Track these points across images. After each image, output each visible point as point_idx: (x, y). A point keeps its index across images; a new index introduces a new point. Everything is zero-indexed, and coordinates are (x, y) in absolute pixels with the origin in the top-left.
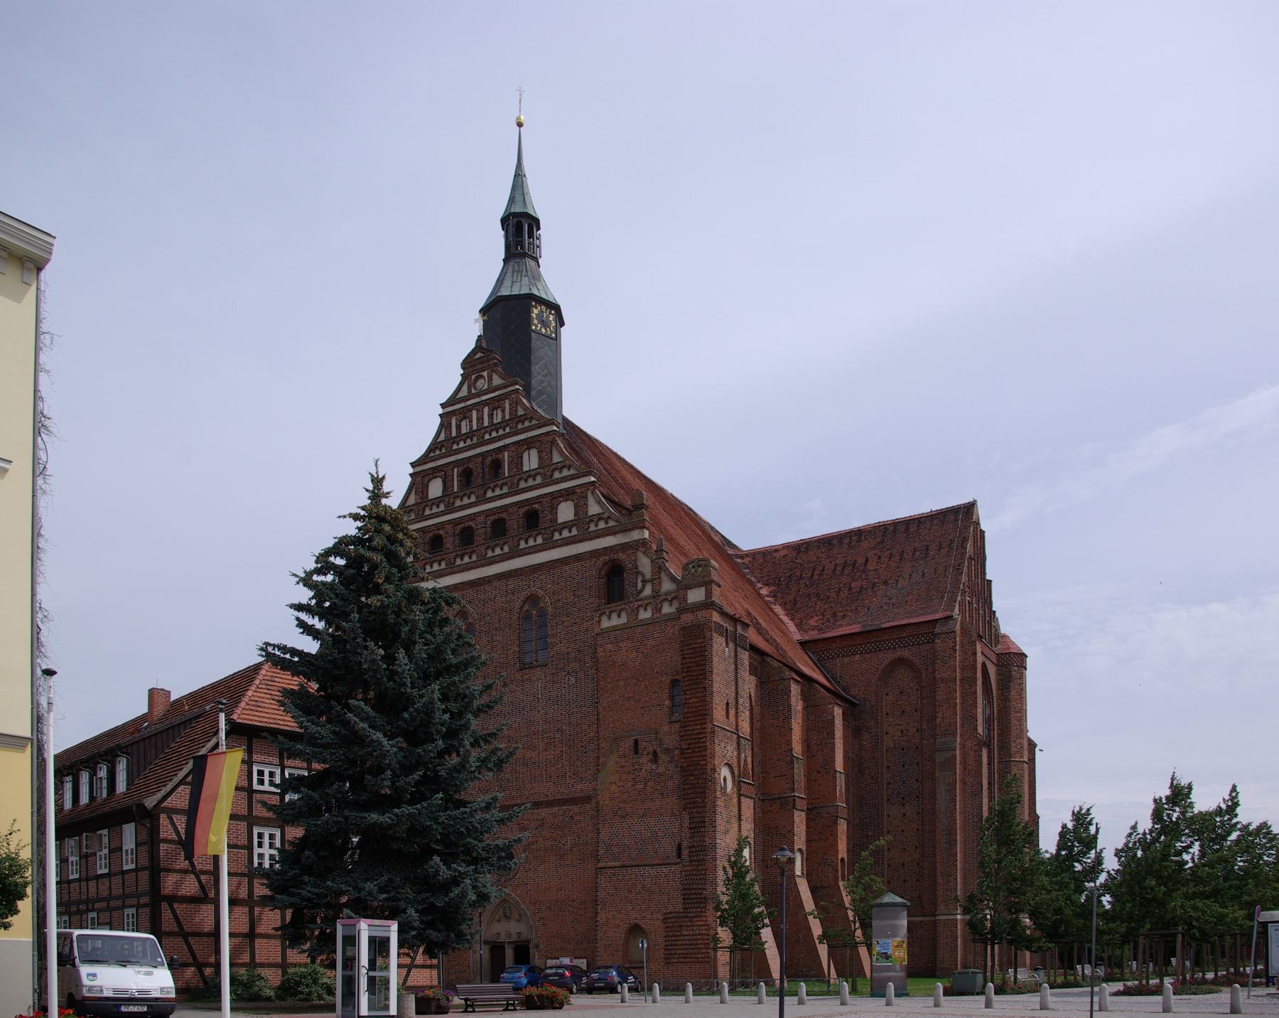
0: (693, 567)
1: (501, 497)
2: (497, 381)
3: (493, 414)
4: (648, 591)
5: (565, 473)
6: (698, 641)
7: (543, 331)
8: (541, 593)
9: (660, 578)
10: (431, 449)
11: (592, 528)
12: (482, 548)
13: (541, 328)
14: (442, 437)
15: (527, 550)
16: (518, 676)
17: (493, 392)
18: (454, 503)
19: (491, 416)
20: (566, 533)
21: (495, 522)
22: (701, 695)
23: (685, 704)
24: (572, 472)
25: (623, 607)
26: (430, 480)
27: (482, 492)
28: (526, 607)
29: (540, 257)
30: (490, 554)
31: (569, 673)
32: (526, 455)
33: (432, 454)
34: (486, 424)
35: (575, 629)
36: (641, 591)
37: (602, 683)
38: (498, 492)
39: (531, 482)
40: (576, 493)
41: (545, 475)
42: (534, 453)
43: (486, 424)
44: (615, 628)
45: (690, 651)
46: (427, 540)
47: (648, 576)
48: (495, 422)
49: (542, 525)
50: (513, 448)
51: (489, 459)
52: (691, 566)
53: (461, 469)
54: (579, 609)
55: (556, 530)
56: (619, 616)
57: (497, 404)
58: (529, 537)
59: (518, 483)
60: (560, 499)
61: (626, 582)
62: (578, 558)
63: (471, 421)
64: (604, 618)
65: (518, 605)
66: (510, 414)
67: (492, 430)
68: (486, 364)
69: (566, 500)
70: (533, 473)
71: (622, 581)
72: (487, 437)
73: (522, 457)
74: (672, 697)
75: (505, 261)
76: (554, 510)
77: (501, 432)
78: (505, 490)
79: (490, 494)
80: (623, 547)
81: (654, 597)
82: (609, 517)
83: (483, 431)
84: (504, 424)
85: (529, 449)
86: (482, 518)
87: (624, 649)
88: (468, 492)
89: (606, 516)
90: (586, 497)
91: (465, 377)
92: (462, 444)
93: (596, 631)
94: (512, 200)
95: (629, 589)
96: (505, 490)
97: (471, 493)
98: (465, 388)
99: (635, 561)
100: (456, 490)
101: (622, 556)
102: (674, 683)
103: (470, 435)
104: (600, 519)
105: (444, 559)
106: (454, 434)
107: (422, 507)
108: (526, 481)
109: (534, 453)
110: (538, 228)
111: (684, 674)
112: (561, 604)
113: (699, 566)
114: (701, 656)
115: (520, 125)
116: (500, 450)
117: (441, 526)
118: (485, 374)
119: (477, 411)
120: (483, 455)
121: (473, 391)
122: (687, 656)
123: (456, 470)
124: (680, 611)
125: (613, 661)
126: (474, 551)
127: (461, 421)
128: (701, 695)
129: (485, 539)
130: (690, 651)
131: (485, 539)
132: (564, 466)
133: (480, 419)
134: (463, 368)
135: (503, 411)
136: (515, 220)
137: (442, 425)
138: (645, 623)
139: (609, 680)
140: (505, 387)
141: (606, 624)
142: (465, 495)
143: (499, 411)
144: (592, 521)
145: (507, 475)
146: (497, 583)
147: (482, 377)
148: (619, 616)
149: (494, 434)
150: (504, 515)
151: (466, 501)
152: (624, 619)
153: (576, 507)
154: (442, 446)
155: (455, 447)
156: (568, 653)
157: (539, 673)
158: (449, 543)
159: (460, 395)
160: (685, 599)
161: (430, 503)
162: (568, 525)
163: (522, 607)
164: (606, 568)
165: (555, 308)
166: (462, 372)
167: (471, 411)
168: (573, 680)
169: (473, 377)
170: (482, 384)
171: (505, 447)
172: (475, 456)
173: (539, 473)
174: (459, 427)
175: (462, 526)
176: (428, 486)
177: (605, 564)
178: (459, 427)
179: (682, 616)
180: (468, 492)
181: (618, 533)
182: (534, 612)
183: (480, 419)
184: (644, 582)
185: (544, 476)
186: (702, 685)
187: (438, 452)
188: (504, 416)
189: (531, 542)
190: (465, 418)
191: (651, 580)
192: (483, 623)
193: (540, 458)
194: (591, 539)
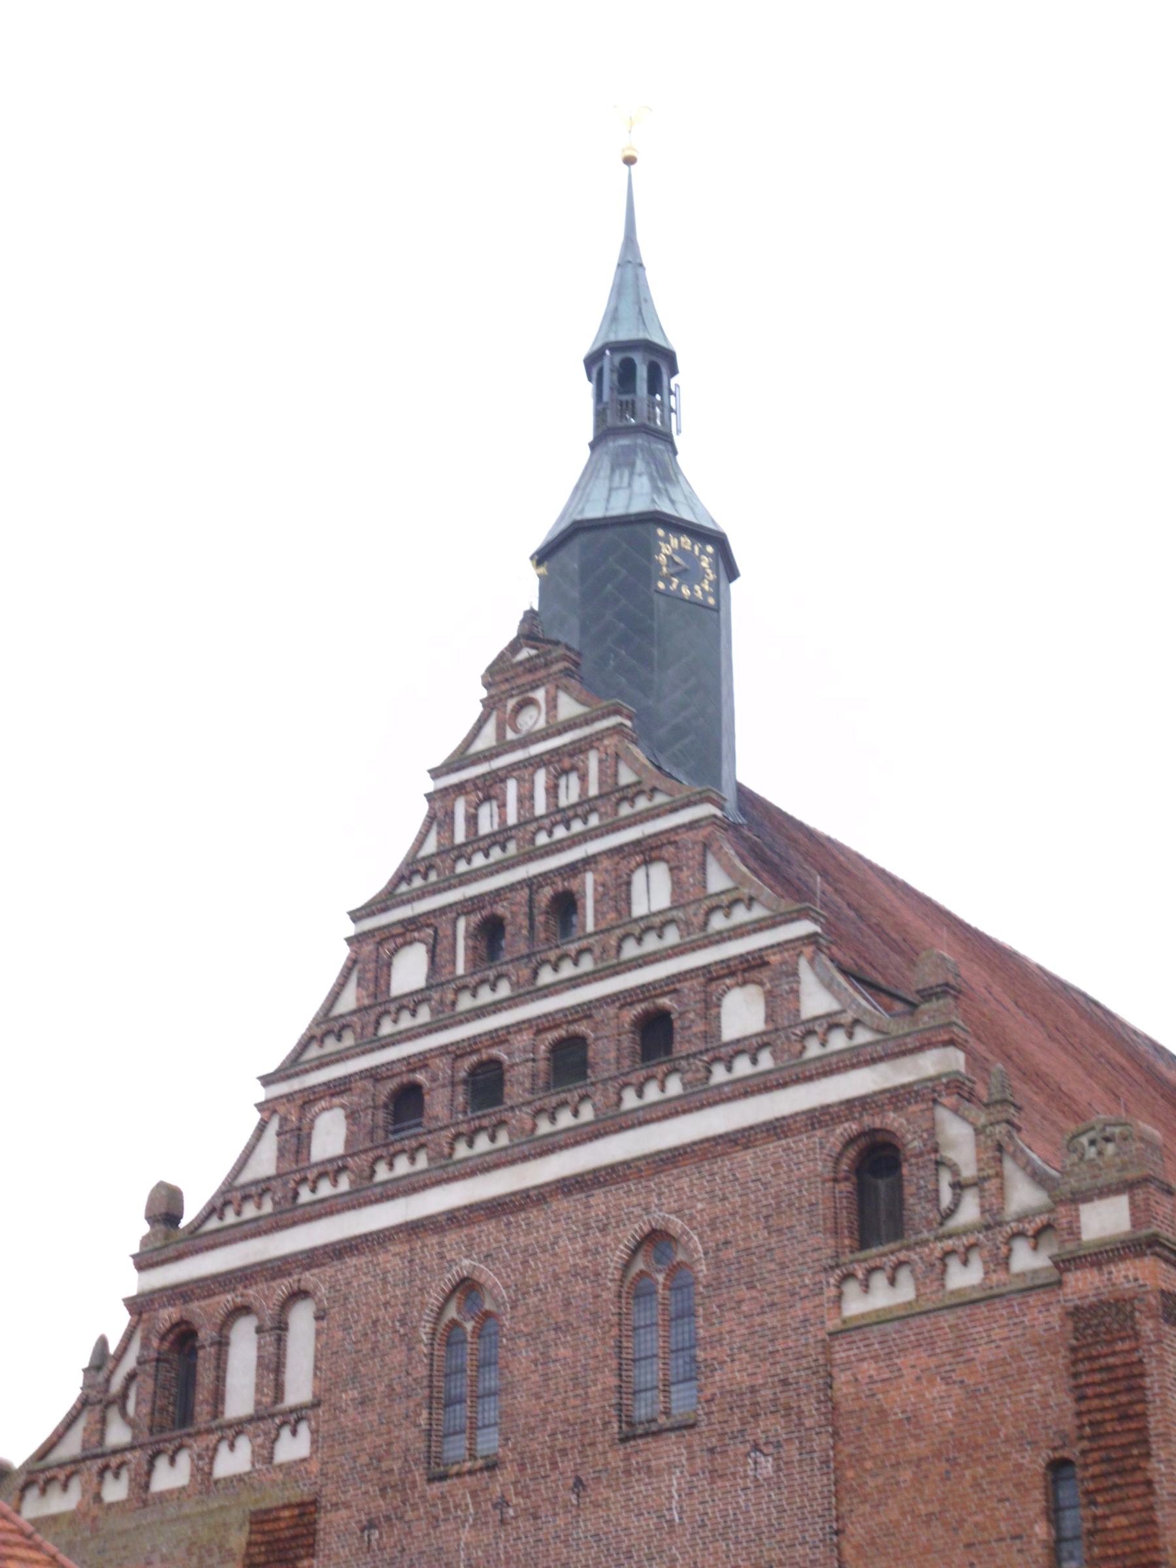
0: (1092, 1142)
1: (574, 983)
2: (568, 707)
3: (556, 787)
4: (969, 1212)
5: (741, 915)
6: (1120, 1346)
7: (686, 591)
8: (677, 1225)
9: (999, 1175)
10: (401, 877)
11: (813, 1049)
12: (525, 1114)
13: (679, 586)
14: (430, 847)
15: (641, 1113)
16: (615, 1459)
17: (559, 732)
18: (454, 1004)
19: (553, 791)
20: (743, 1067)
21: (558, 1048)
22: (1138, 1504)
23: (1091, 1533)
24: (758, 912)
25: (902, 1255)
26: (396, 950)
27: (526, 973)
28: (639, 1265)
29: (679, 432)
30: (544, 1127)
31: (756, 1447)
32: (639, 878)
33: (404, 888)
34: (540, 808)
35: (771, 1319)
36: (951, 1212)
37: (850, 1474)
38: (568, 970)
39: (652, 943)
40: (766, 964)
41: (688, 924)
42: (660, 874)
43: (540, 808)
44: (881, 1319)
45: (1097, 1377)
46: (382, 1099)
47: (969, 1171)
48: (563, 802)
49: (680, 1048)
50: (606, 863)
51: (548, 892)
52: (1084, 1140)
53: (476, 918)
54: (783, 1266)
55: (716, 1059)
56: (892, 1281)
57: (567, 762)
58: (649, 1078)
59: (619, 948)
60: (728, 981)
61: (909, 1189)
62: (776, 1129)
63: (503, 806)
64: (852, 1289)
65: (619, 1255)
66: (601, 783)
67: (554, 824)
68: (542, 673)
69: (744, 983)
70: (657, 921)
71: (898, 1188)
72: (542, 839)
73: (629, 884)
74: (1054, 1513)
75: (593, 446)
76: (710, 1008)
77: (577, 826)
78: (587, 964)
79: (547, 976)
80: (897, 1097)
81: (988, 1227)
82: (856, 1022)
83: (532, 827)
84: (585, 807)
85: (647, 862)
86: (526, 1038)
87: (909, 1375)
88: (491, 974)
89: (847, 1018)
90: (795, 973)
91: (490, 705)
92: (479, 861)
93: (832, 1324)
94: (613, 317)
95: (916, 1208)
96: (587, 964)
97: (500, 976)
98: (490, 730)
99: (932, 1131)
100: (460, 969)
101: (893, 1120)
102: (1058, 1467)
103: (501, 837)
104: (833, 1026)
105: (422, 1146)
106: (460, 837)
107: (373, 1018)
108: (639, 940)
109: (660, 874)
110: (674, 371)
111: (1085, 1444)
112: (732, 1253)
113: (1108, 1140)
114: (1129, 1390)
115: (629, 161)
116: (574, 869)
117: (421, 1061)
118: (540, 695)
119: (520, 780)
120: (533, 884)
121: (510, 735)
122: (1089, 1391)
123: (462, 924)
124: (1064, 1264)
125: (882, 1412)
126: (502, 1123)
127: (477, 806)
128: (1138, 1504)
129: (532, 1091)
130: (1097, 1377)
131: (532, 1091)
132: (736, 901)
133: (526, 799)
134: (487, 685)
135: (583, 778)
136: (618, 358)
137: (431, 819)
138: (967, 1302)
139: (869, 1464)
140: (587, 721)
141: (856, 1305)
142: (483, 982)
143: (574, 778)
144: (811, 1033)
145: (590, 927)
146: (561, 1205)
147: (532, 702)
148: (892, 1281)
149: (560, 833)
150: (582, 1028)
151: (486, 996)
152: (906, 1292)
153: (771, 998)
154: (431, 867)
155: (462, 867)
156: (753, 1390)
157: (671, 1449)
158: (438, 1104)
159: (480, 745)
160: (1074, 1231)
161: (393, 1007)
162: (749, 1047)
163: (627, 1266)
164: (852, 1152)
165: (719, 541)
166: (484, 693)
167: (503, 780)
168: (767, 1466)
169: (511, 703)
170: (533, 720)
171: (588, 862)
172: (512, 887)
173: (672, 921)
174: (472, 820)
175: (474, 1058)
176: (389, 965)
177: (850, 1142)
178: (472, 820)
179: (1070, 1278)
180: (491, 974)
181: (880, 1059)
182: (660, 1278)
183: (526, 799)
184: (959, 1186)
185: (686, 926)
186: (1139, 1476)
187: (418, 882)
188: (584, 789)
189: (652, 1093)
190: (488, 798)
191: (977, 1183)
192: (521, 1310)
193: (676, 884)
194: (809, 1078)
